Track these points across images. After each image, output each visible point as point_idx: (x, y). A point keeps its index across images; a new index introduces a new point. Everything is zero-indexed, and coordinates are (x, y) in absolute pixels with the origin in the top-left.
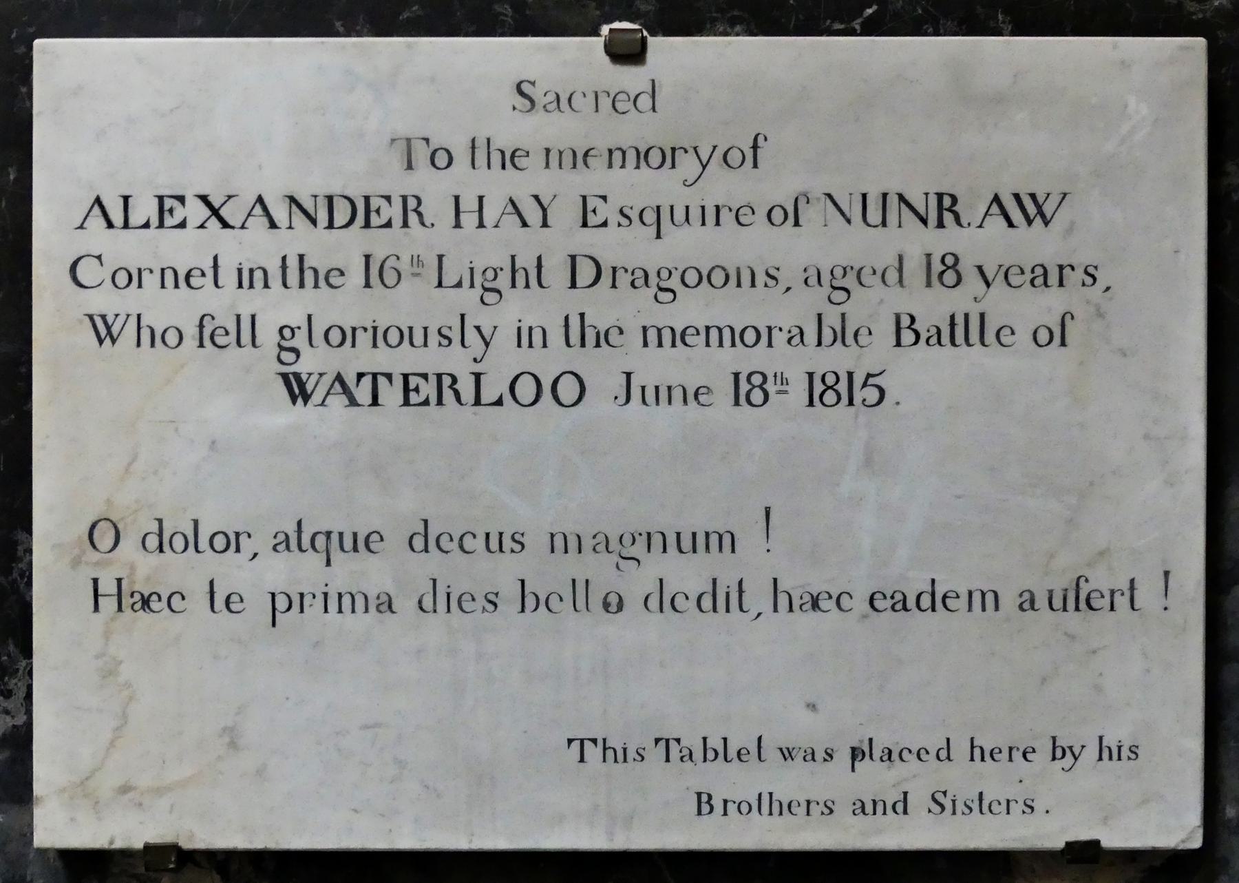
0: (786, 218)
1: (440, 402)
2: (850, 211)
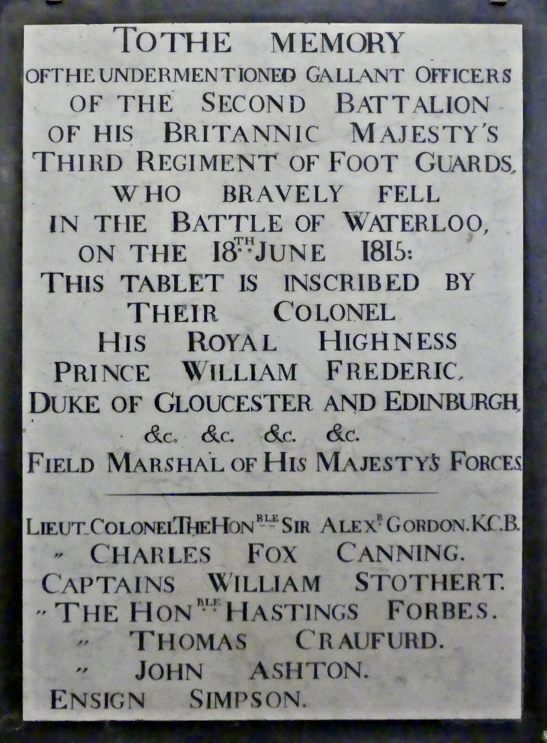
0: (414, 527)
1: (161, 80)
2: (122, 461)
